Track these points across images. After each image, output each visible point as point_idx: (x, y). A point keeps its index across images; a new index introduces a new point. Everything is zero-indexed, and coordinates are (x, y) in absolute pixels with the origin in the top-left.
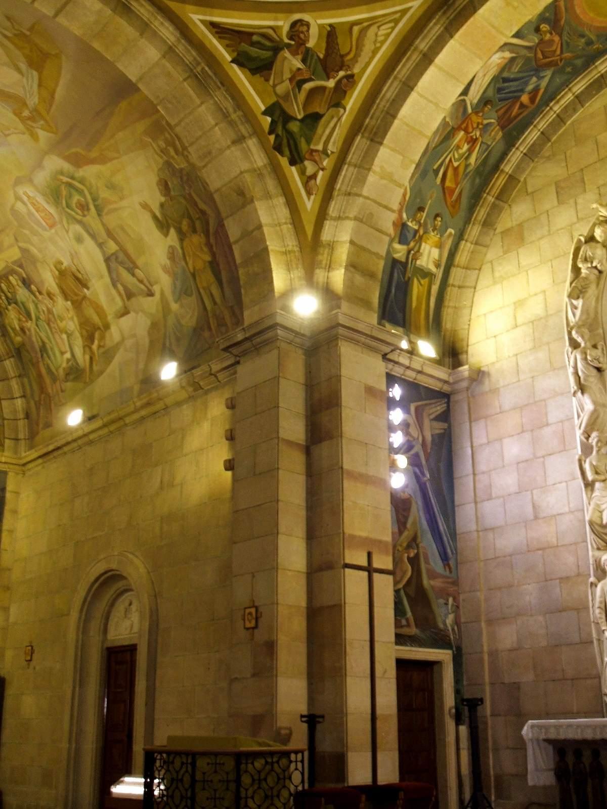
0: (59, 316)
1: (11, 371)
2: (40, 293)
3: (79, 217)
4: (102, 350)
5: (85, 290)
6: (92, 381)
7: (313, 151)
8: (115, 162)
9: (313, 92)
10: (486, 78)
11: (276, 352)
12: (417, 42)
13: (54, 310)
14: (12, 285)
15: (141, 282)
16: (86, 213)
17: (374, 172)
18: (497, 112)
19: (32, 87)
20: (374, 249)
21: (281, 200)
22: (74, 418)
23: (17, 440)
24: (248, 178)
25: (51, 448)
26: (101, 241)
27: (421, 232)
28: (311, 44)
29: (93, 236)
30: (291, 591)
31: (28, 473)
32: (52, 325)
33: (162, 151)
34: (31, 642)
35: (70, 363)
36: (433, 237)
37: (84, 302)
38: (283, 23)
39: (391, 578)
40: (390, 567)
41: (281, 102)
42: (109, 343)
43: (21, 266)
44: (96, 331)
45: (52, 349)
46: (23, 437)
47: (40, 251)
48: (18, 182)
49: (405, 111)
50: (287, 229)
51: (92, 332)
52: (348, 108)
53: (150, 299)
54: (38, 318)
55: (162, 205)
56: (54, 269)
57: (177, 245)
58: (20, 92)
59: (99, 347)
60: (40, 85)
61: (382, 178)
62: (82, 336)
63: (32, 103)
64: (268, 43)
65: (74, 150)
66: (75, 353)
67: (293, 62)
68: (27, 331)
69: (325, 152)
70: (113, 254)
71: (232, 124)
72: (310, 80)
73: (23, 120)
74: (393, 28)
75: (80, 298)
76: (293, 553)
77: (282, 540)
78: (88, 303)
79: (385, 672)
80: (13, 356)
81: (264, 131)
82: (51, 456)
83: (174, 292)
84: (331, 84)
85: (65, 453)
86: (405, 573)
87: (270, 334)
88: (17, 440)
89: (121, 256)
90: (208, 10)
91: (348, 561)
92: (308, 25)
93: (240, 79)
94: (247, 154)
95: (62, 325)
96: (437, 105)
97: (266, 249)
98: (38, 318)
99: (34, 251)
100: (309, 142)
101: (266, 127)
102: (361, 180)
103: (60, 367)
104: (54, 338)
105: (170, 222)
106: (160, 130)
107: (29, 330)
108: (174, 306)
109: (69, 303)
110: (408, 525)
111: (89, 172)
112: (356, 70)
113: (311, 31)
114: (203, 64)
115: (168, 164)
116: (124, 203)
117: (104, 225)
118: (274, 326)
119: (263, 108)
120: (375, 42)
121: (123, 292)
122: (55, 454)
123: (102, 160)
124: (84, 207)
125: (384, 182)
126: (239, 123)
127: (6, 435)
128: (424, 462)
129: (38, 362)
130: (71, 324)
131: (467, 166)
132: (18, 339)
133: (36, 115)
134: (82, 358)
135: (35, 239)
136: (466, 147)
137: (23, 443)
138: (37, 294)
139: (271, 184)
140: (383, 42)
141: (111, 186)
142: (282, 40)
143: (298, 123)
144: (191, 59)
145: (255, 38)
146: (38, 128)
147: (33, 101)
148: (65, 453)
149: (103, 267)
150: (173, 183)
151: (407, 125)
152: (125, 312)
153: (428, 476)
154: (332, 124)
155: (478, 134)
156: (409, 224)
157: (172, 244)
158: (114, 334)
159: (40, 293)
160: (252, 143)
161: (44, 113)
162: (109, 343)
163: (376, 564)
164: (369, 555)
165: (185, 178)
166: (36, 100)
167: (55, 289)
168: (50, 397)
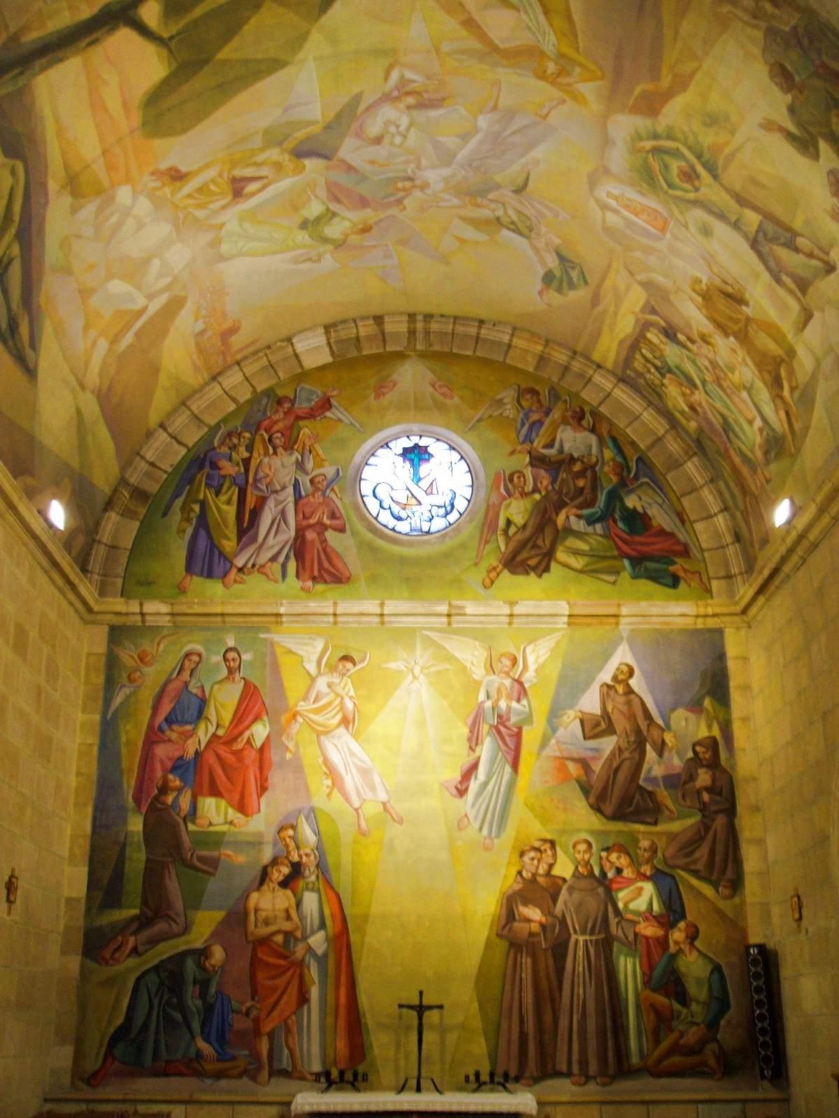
0: (727, 367)
1: (696, 474)
2: (693, 342)
3: (692, 196)
4: (797, 394)
5: (744, 308)
6: (798, 450)
8: (699, 76)
13: (718, 359)
14: (655, 345)
15: (810, 255)
16: (697, 183)
19: (537, 19)
22: (781, 513)
23: (729, 577)
25: (766, 573)
26: (733, 218)
29: (722, 216)
32: (725, 384)
33: (755, 17)
34: (796, 889)
35: (765, 433)
37: (749, 328)
42: (802, 377)
43: (653, 311)
44: (779, 366)
45: (736, 422)
46: (737, 572)
48: (593, 181)
51: (775, 370)
53: (833, 276)
54: (704, 382)
55: (791, 110)
56: (694, 295)
59: (792, 389)
62: (765, 384)
63: (550, 47)
65: (638, 90)
66: (765, 415)
68: (698, 408)
70: (757, 231)
75: (741, 325)
78: (755, 327)
80: (695, 454)
82: (772, 588)
85: (788, 576)
89: (770, 228)
95: (735, 378)
98: (704, 382)
99: (659, 279)
103: (754, 445)
104: (731, 401)
105: (811, 129)
107: (700, 404)
109: (732, 339)
111: (673, 113)
115: (771, 33)
116: (738, 138)
117: (728, 191)
121: (793, 286)
122: (777, 581)
123: (681, 84)
124: (690, 176)
127: (711, 573)
129: (727, 450)
130: (746, 372)
133: (565, 65)
134: (777, 421)
135: (652, 260)
138: (689, 344)
141: (712, 120)
146: (577, 82)
147: (550, 42)
149: (752, 257)
150: (793, 61)
157: (832, 165)
158: (804, 362)
159: (693, 342)
161: (570, 52)
162: (802, 377)
165: (806, 42)
166: (553, 38)
167: (706, 326)
168: (756, 498)
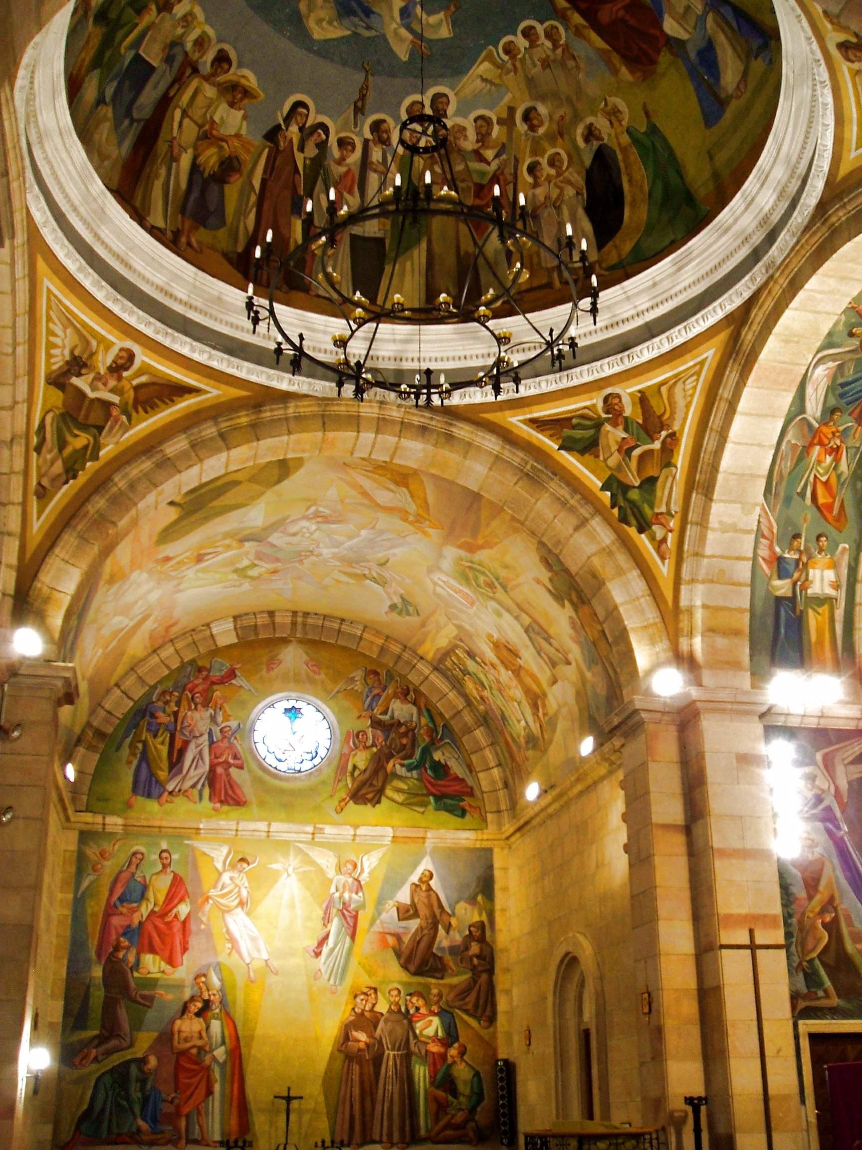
3: (491, 595)
7: (657, 514)
9: (642, 457)
10: (819, 392)
11: (643, 736)
12: (721, 391)
17: (713, 530)
18: (850, 414)
20: (735, 604)
21: (635, 573)
24: (596, 561)
27: (805, 559)
28: (628, 412)
29: (508, 610)
30: (677, 974)
31: (514, 847)
36: (821, 559)
38: (596, 400)
39: (783, 952)
40: (781, 941)
41: (616, 474)
42: (551, 711)
43: (461, 640)
47: (471, 625)
48: (430, 571)
49: (727, 461)
50: (646, 602)
51: (536, 700)
52: (679, 466)
54: (491, 688)
55: (551, 580)
57: (573, 614)
58: (400, 505)
59: (545, 714)
60: (412, 496)
61: (724, 531)
64: (588, 423)
65: (463, 540)
67: (614, 435)
69: (669, 513)
71: (572, 510)
72: (637, 446)
73: (411, 523)
74: (697, 380)
76: (676, 936)
77: (663, 928)
79: (779, 1051)
81: (604, 505)
83: (584, 660)
84: (657, 445)
86: (819, 941)
87: (636, 719)
88: (499, 811)
89: (536, 628)
90: (526, 409)
91: (724, 941)
92: (618, 396)
93: (571, 463)
94: (593, 537)
96: (759, 445)
97: (625, 629)
98: (491, 688)
99: (467, 627)
100: (652, 507)
101: (608, 502)
102: (702, 539)
106: (518, 524)
108: (589, 675)
110: (821, 888)
111: (483, 555)
112: (676, 427)
113: (623, 400)
114: (531, 462)
116: (520, 580)
118: (636, 712)
119: (600, 485)
120: (685, 397)
124: (491, 586)
125: (728, 535)
126: (579, 507)
128: (838, 814)
130: (517, 693)
131: (839, 476)
132: (482, 708)
134: (535, 729)
136: (829, 459)
137: (506, 814)
139: (622, 559)
140: (692, 396)
141: (506, 567)
142: (599, 416)
143: (636, 490)
144: (518, 460)
145: (574, 421)
147: (412, 508)
148: (534, 827)
149: (524, 635)
151: (733, 474)
152: (554, 682)
153: (846, 829)
154: (668, 485)
155: (838, 442)
156: (787, 556)
160: (597, 524)
162: (551, 711)
163: (759, 941)
164: (751, 932)
167: (495, 660)
